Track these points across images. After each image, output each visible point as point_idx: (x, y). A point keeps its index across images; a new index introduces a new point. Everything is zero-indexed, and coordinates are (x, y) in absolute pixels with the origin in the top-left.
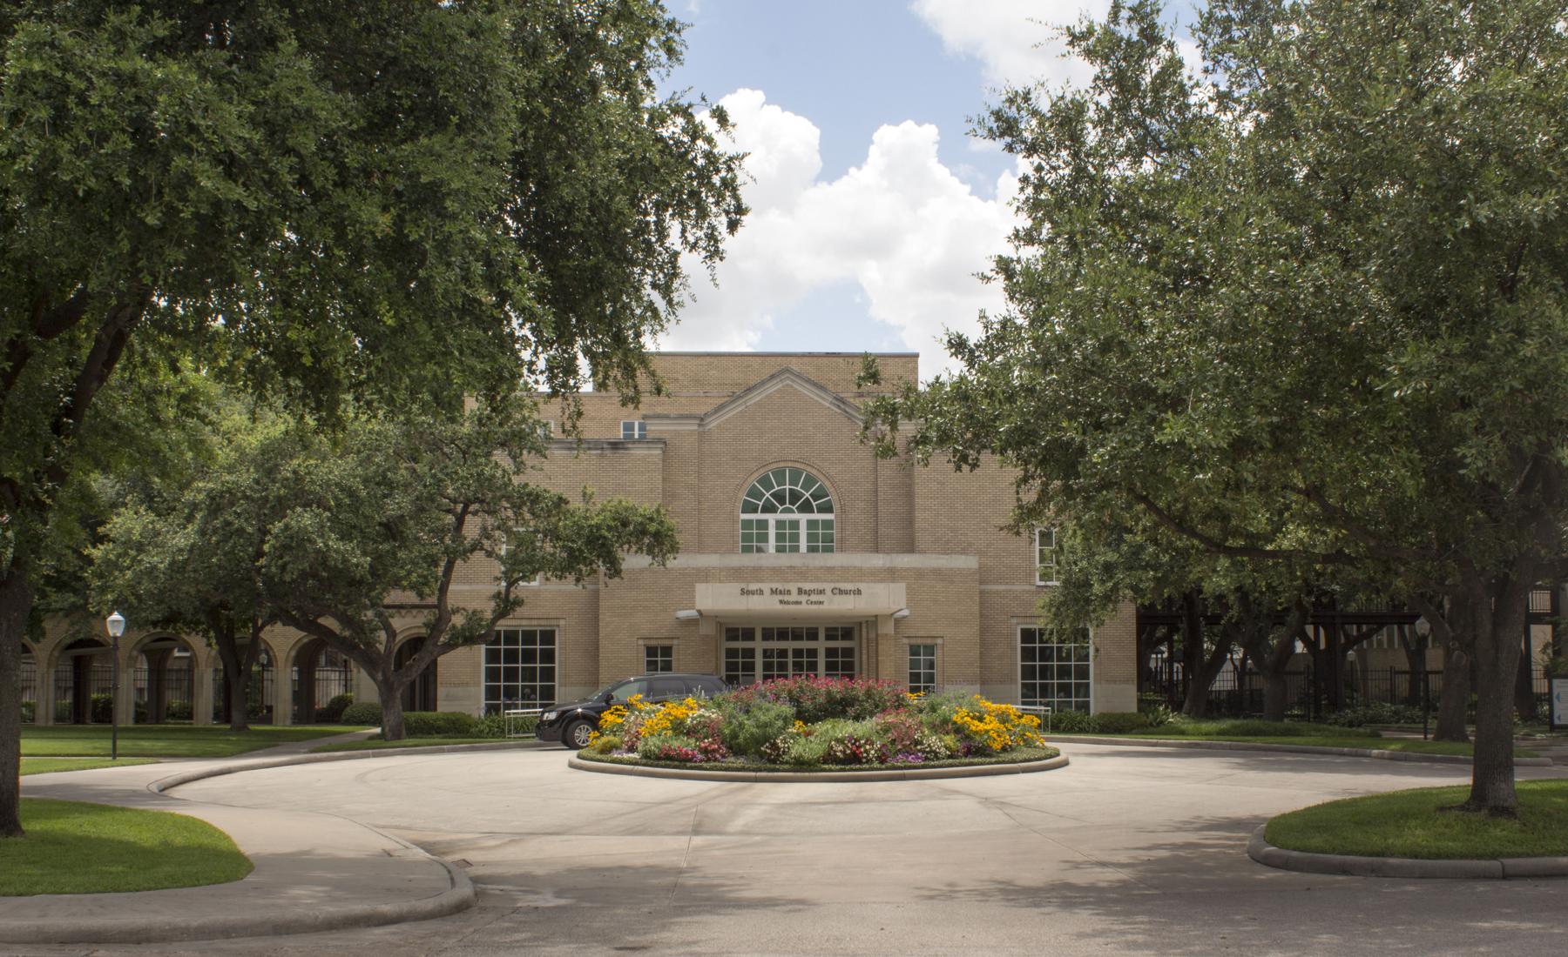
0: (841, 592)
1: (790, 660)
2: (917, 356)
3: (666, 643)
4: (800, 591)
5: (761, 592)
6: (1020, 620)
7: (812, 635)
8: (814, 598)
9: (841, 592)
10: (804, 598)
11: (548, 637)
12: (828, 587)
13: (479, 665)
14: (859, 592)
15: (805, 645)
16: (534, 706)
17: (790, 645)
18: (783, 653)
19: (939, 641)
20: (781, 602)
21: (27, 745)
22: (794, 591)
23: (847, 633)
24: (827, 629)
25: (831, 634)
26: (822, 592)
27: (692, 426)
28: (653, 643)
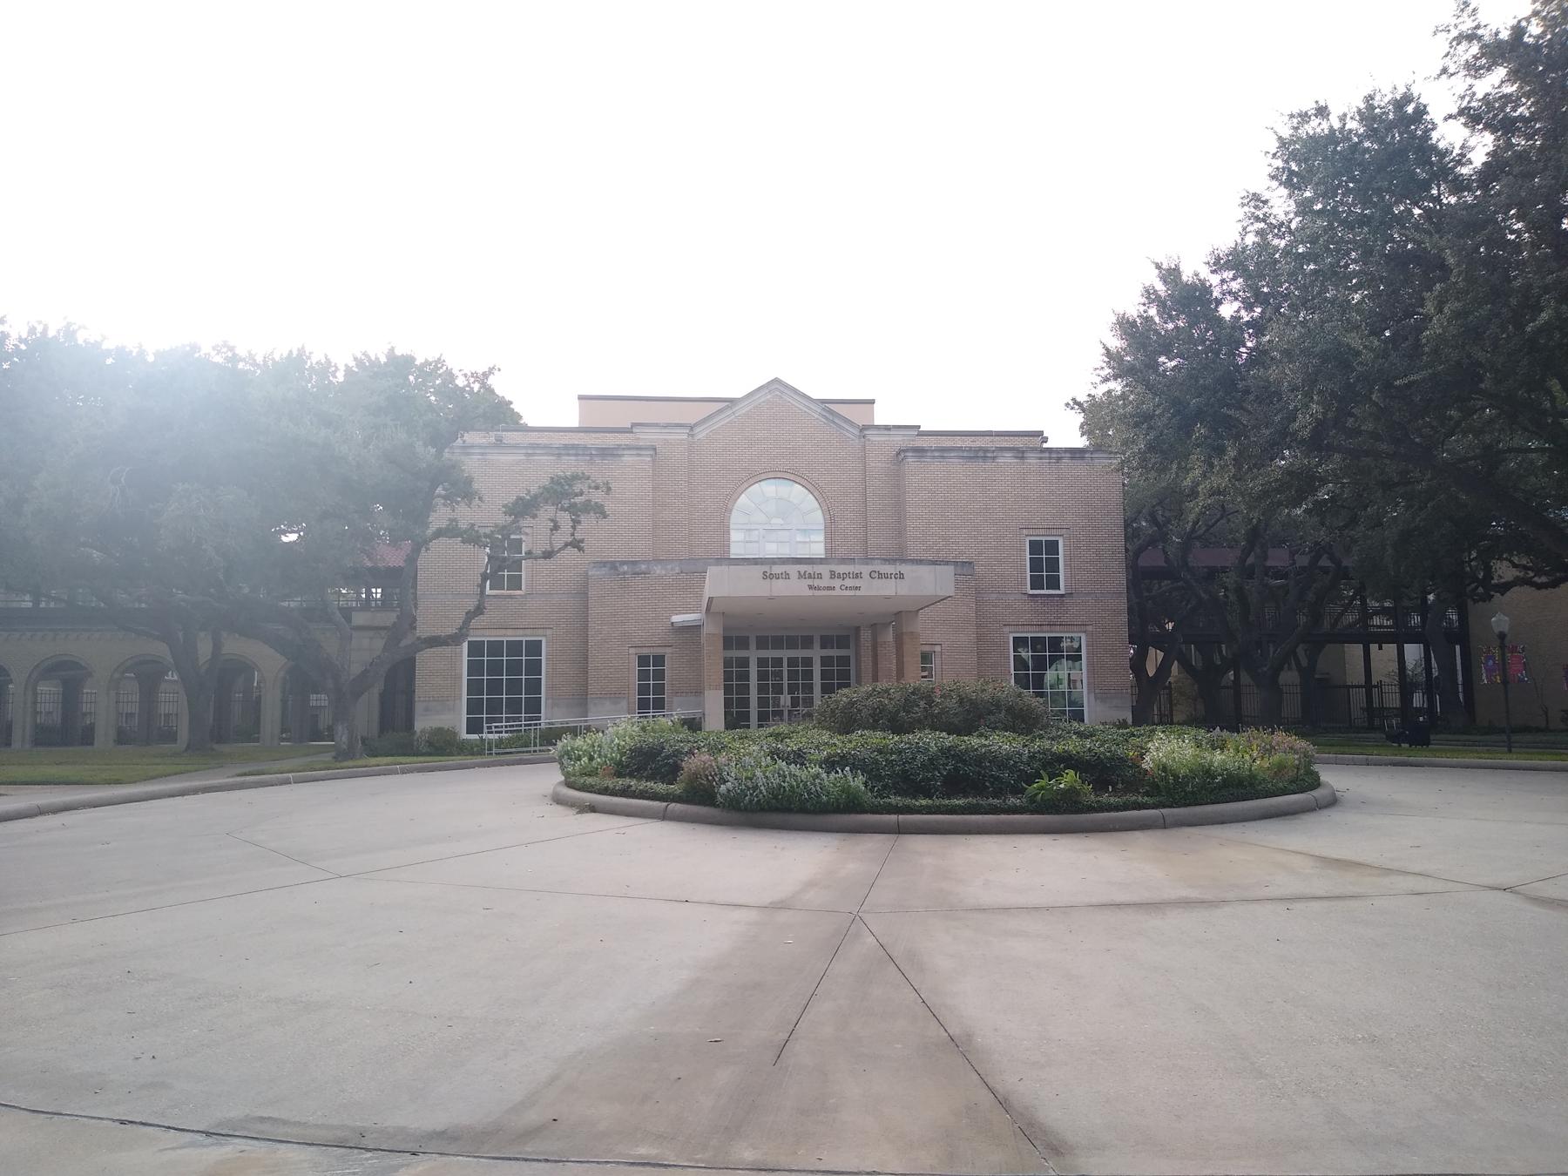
0: (881, 576)
1: (785, 669)
2: (872, 402)
3: (660, 651)
4: (833, 575)
5: (787, 576)
6: (1012, 628)
7: (807, 642)
8: (849, 582)
9: (881, 576)
10: (837, 583)
11: (535, 648)
12: (865, 569)
13: (461, 677)
14: (901, 576)
15: (800, 653)
16: (519, 719)
17: (785, 654)
18: (778, 662)
19: (938, 649)
20: (810, 587)
21: (1422, 645)
22: (826, 575)
23: (842, 642)
24: (822, 637)
25: (826, 642)
26: (857, 576)
27: (682, 435)
28: (645, 651)
